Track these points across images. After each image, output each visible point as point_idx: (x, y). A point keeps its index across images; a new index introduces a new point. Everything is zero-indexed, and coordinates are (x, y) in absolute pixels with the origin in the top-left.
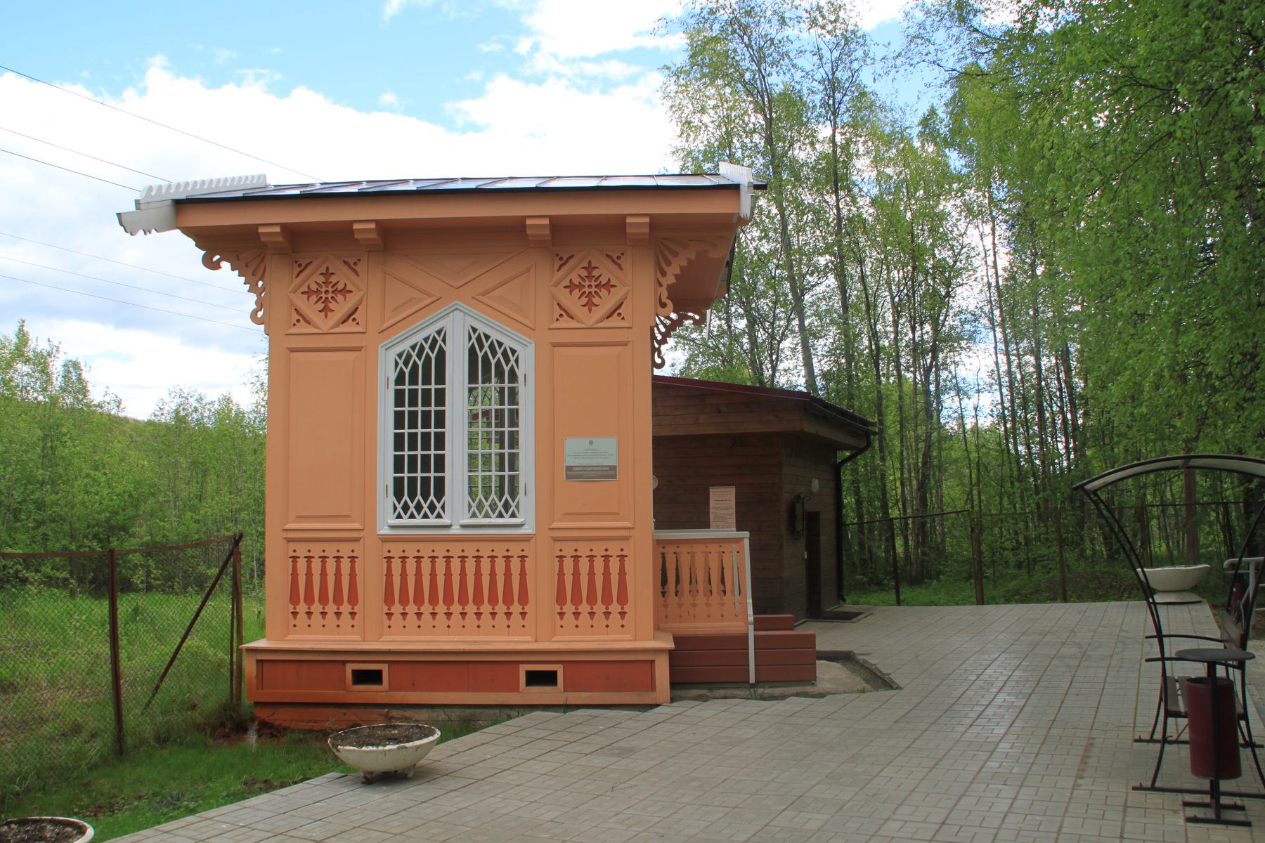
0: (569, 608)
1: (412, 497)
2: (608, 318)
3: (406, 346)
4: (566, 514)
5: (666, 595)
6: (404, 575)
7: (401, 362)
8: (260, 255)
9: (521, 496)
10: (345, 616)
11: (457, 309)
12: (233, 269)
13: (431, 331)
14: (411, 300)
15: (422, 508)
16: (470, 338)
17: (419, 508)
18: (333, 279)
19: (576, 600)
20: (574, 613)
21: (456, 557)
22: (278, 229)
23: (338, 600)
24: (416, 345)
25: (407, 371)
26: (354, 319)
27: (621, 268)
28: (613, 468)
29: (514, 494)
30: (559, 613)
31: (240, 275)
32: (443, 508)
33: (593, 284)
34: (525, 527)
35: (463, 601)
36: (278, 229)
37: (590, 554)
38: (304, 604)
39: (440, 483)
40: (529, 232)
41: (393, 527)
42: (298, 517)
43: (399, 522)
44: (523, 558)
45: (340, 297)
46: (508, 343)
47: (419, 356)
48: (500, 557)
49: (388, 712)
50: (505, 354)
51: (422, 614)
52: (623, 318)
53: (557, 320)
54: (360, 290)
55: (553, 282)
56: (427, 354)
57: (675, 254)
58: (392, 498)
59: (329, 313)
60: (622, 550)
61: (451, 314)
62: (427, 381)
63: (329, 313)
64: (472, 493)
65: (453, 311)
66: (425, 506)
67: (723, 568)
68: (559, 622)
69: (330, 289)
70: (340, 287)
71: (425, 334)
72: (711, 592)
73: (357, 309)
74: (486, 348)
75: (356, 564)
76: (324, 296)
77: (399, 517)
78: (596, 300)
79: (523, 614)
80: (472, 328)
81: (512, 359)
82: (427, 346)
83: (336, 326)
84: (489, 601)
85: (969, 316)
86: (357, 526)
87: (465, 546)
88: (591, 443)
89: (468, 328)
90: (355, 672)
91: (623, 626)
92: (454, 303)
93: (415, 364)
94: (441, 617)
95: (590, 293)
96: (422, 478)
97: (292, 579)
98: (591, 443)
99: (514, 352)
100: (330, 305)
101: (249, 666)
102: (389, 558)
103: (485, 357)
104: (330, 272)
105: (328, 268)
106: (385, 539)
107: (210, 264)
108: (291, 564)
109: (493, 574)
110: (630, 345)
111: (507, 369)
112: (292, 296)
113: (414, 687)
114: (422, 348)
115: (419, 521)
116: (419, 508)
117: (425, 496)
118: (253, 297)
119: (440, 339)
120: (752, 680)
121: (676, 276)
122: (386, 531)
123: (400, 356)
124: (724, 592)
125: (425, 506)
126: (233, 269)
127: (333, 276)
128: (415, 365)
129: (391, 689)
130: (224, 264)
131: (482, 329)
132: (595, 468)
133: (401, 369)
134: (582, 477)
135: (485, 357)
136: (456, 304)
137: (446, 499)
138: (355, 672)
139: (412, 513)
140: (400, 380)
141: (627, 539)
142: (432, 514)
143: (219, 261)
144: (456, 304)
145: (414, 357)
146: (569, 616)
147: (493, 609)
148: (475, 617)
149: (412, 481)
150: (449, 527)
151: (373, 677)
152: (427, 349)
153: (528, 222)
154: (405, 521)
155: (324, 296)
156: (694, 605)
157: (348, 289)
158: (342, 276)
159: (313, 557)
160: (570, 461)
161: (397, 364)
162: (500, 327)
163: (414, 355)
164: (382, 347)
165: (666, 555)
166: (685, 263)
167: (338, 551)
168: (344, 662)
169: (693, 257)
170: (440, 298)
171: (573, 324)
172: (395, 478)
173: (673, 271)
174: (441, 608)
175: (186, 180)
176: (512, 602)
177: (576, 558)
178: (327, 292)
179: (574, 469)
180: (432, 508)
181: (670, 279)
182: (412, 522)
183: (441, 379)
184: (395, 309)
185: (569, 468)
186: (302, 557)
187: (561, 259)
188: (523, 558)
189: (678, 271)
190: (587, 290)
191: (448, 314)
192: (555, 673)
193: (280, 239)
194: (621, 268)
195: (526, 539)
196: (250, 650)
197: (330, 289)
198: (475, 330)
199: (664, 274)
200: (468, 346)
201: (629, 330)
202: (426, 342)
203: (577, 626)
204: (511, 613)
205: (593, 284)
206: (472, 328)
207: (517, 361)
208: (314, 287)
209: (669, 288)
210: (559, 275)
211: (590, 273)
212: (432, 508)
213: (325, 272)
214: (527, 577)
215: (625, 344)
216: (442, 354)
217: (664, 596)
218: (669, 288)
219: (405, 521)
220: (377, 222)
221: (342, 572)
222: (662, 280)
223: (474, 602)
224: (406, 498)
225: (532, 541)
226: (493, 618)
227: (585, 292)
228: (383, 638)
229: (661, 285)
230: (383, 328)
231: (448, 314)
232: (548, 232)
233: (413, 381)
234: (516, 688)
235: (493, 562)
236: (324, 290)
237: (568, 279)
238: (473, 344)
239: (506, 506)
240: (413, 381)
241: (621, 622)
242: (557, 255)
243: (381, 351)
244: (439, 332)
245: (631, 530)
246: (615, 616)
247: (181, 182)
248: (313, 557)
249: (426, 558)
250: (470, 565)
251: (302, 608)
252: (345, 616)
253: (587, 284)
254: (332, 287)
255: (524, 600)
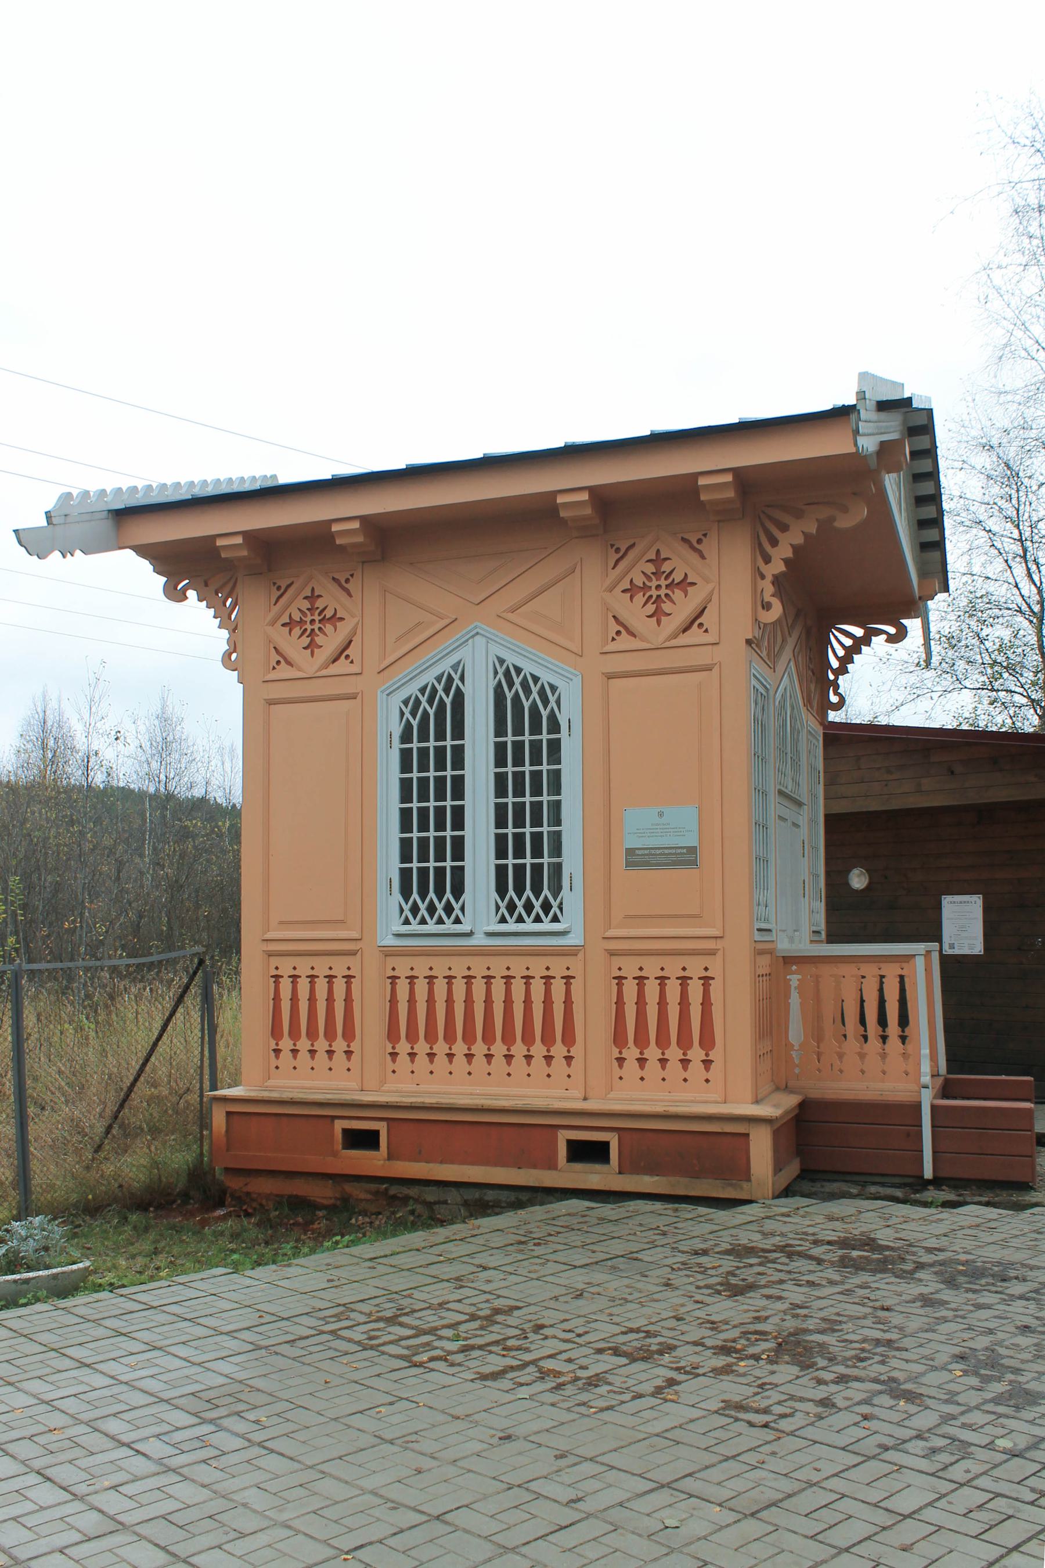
0: (632, 1053)
1: (423, 895)
2: (685, 631)
3: (412, 689)
4: (627, 917)
5: (907, 1041)
6: (294, 999)
7: (407, 712)
8: (231, 578)
9: (565, 892)
10: (339, 1056)
11: (477, 633)
12: (200, 600)
13: (445, 666)
14: (419, 624)
15: (436, 909)
16: (496, 673)
17: (432, 909)
18: (320, 604)
19: (641, 1041)
20: (505, 1056)
21: (630, 978)
22: (239, 540)
23: (548, 1039)
24: (426, 687)
25: (415, 723)
26: (278, 663)
27: (703, 557)
28: (692, 850)
29: (556, 889)
30: (617, 1059)
31: (208, 607)
32: (462, 909)
33: (663, 583)
34: (570, 935)
35: (528, 1039)
36: (239, 540)
37: (347, 973)
38: (288, 1039)
39: (459, 873)
40: (563, 514)
41: (398, 935)
42: (281, 923)
43: (406, 928)
44: (706, 980)
45: (328, 628)
46: (546, 677)
47: (430, 702)
48: (479, 977)
49: (386, 1189)
50: (542, 693)
51: (512, 1056)
52: (706, 631)
53: (613, 639)
54: (707, 581)
55: (608, 582)
56: (441, 699)
57: (784, 528)
58: (397, 897)
59: (664, 619)
60: (641, 969)
61: (470, 641)
62: (440, 736)
63: (664, 619)
64: (501, 890)
65: (473, 637)
66: (440, 907)
67: (862, 1001)
68: (391, 1066)
69: (317, 618)
70: (329, 613)
71: (437, 671)
72: (845, 1036)
73: (351, 642)
74: (517, 685)
75: (353, 986)
76: (309, 627)
77: (407, 922)
78: (666, 607)
79: (569, 1059)
80: (498, 658)
81: (552, 699)
82: (440, 688)
83: (675, 636)
84: (445, 1038)
85: (1015, 606)
86: (355, 935)
87: (491, 961)
88: (661, 814)
89: (492, 658)
90: (346, 1132)
91: (707, 1081)
92: (473, 626)
93: (426, 714)
94: (460, 1060)
95: (320, 621)
96: (514, 865)
97: (274, 1004)
98: (661, 814)
99: (553, 688)
100: (316, 638)
101: (219, 1119)
102: (277, 977)
103: (516, 698)
104: (316, 594)
105: (658, 551)
106: (388, 953)
107: (175, 594)
108: (390, 986)
109: (488, 1001)
110: (716, 669)
111: (545, 714)
112: (269, 629)
113: (417, 1156)
114: (434, 691)
115: (431, 927)
116: (432, 909)
117: (440, 893)
118: (225, 634)
119: (456, 678)
120: (928, 1173)
121: (786, 561)
122: (390, 941)
123: (406, 702)
124: (865, 1038)
125: (440, 907)
126: (200, 600)
127: (320, 600)
128: (426, 715)
129: (390, 1157)
130: (192, 594)
131: (511, 659)
132: (666, 851)
133: (408, 720)
134: (647, 864)
135: (516, 698)
136: (476, 627)
137: (466, 897)
138: (346, 1132)
139: (423, 917)
140: (406, 736)
141: (712, 953)
142: (529, 916)
143: (184, 590)
144: (476, 627)
145: (424, 704)
146: (631, 1064)
147: (528, 1050)
148: (485, 1060)
149: (423, 873)
150: (470, 934)
151: (366, 1140)
152: (441, 692)
153: (702, 481)
154: (511, 926)
155: (309, 627)
156: (841, 1056)
157: (338, 616)
158: (331, 599)
159: (533, 977)
160: (631, 842)
161: (402, 714)
162: (535, 655)
163: (424, 700)
164: (382, 692)
165: (906, 980)
166: (799, 540)
167: (313, 968)
168: (334, 1118)
169: (812, 529)
170: (456, 619)
171: (636, 644)
172: (401, 869)
173: (783, 552)
174: (499, 1049)
175: (217, 477)
176: (514, 1041)
177: (684, 980)
178: (312, 621)
179: (637, 852)
180: (449, 909)
181: (777, 567)
182: (424, 929)
183: (459, 732)
184: (398, 639)
185: (630, 852)
186: (322, 977)
187: (617, 550)
188: (706, 980)
189: (789, 553)
190: (654, 593)
191: (467, 640)
192: (376, 1133)
193: (245, 553)
194: (703, 557)
195: (571, 952)
196: (225, 1099)
197: (317, 618)
198: (502, 661)
199: (767, 560)
200: (493, 684)
201: (715, 647)
202: (439, 683)
203: (642, 1079)
204: (552, 1057)
205: (663, 583)
206: (498, 658)
207: (558, 702)
208: (297, 616)
209: (777, 580)
210: (276, 609)
211: (658, 568)
212: (449, 909)
213: (654, 558)
214: (691, 1007)
215: (708, 668)
216: (460, 695)
217: (903, 1043)
218: (777, 580)
219: (415, 927)
220: (591, 490)
221: (455, 998)
222: (764, 568)
223: (563, 1041)
224: (415, 896)
225: (581, 955)
226: (663, 1068)
227: (651, 597)
228: (386, 1087)
229: (763, 577)
230: (383, 666)
231: (467, 640)
232: (730, 494)
233: (424, 737)
234: (551, 1164)
235: (312, 983)
236: (309, 619)
237: (627, 580)
238: (500, 682)
239: (546, 907)
240: (424, 737)
241: (705, 1075)
242: (274, 584)
243: (381, 697)
244: (455, 667)
245: (719, 940)
246: (696, 1066)
247: (169, 483)
248: (533, 977)
249: (340, 977)
250: (538, 988)
251: (286, 1044)
252: (339, 1056)
253: (654, 583)
254: (319, 614)
255: (569, 1038)
